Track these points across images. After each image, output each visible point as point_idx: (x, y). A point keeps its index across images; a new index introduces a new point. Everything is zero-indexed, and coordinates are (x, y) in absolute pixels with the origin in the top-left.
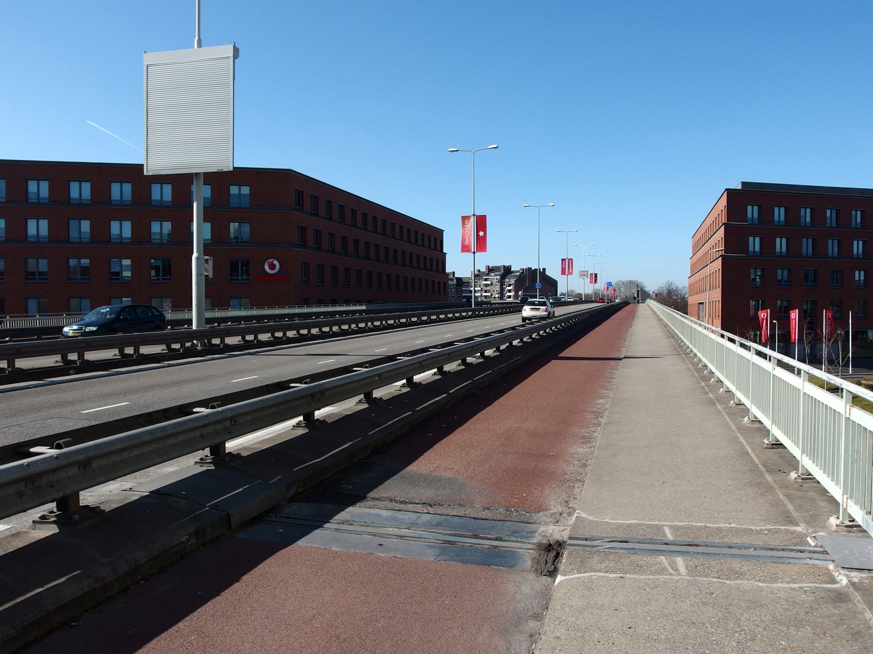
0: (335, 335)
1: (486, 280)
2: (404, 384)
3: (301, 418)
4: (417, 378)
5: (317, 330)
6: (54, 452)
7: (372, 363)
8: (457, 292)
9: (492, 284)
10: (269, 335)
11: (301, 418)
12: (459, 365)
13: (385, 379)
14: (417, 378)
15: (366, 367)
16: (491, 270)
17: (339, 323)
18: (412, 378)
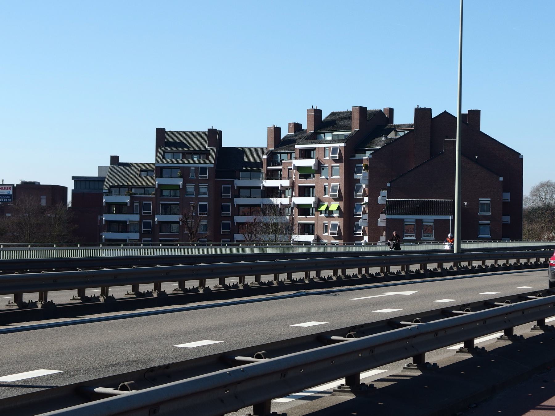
0: (209, 295)
1: (306, 154)
2: (502, 336)
3: (343, 381)
4: (479, 342)
5: (176, 285)
6: (415, 325)
7: (272, 349)
8: (217, 193)
9: (320, 167)
10: (129, 288)
11: (343, 381)
12: (535, 328)
13: (441, 340)
14: (479, 342)
15: (507, 302)
16: (322, 124)
17: (257, 272)
18: (267, 405)
